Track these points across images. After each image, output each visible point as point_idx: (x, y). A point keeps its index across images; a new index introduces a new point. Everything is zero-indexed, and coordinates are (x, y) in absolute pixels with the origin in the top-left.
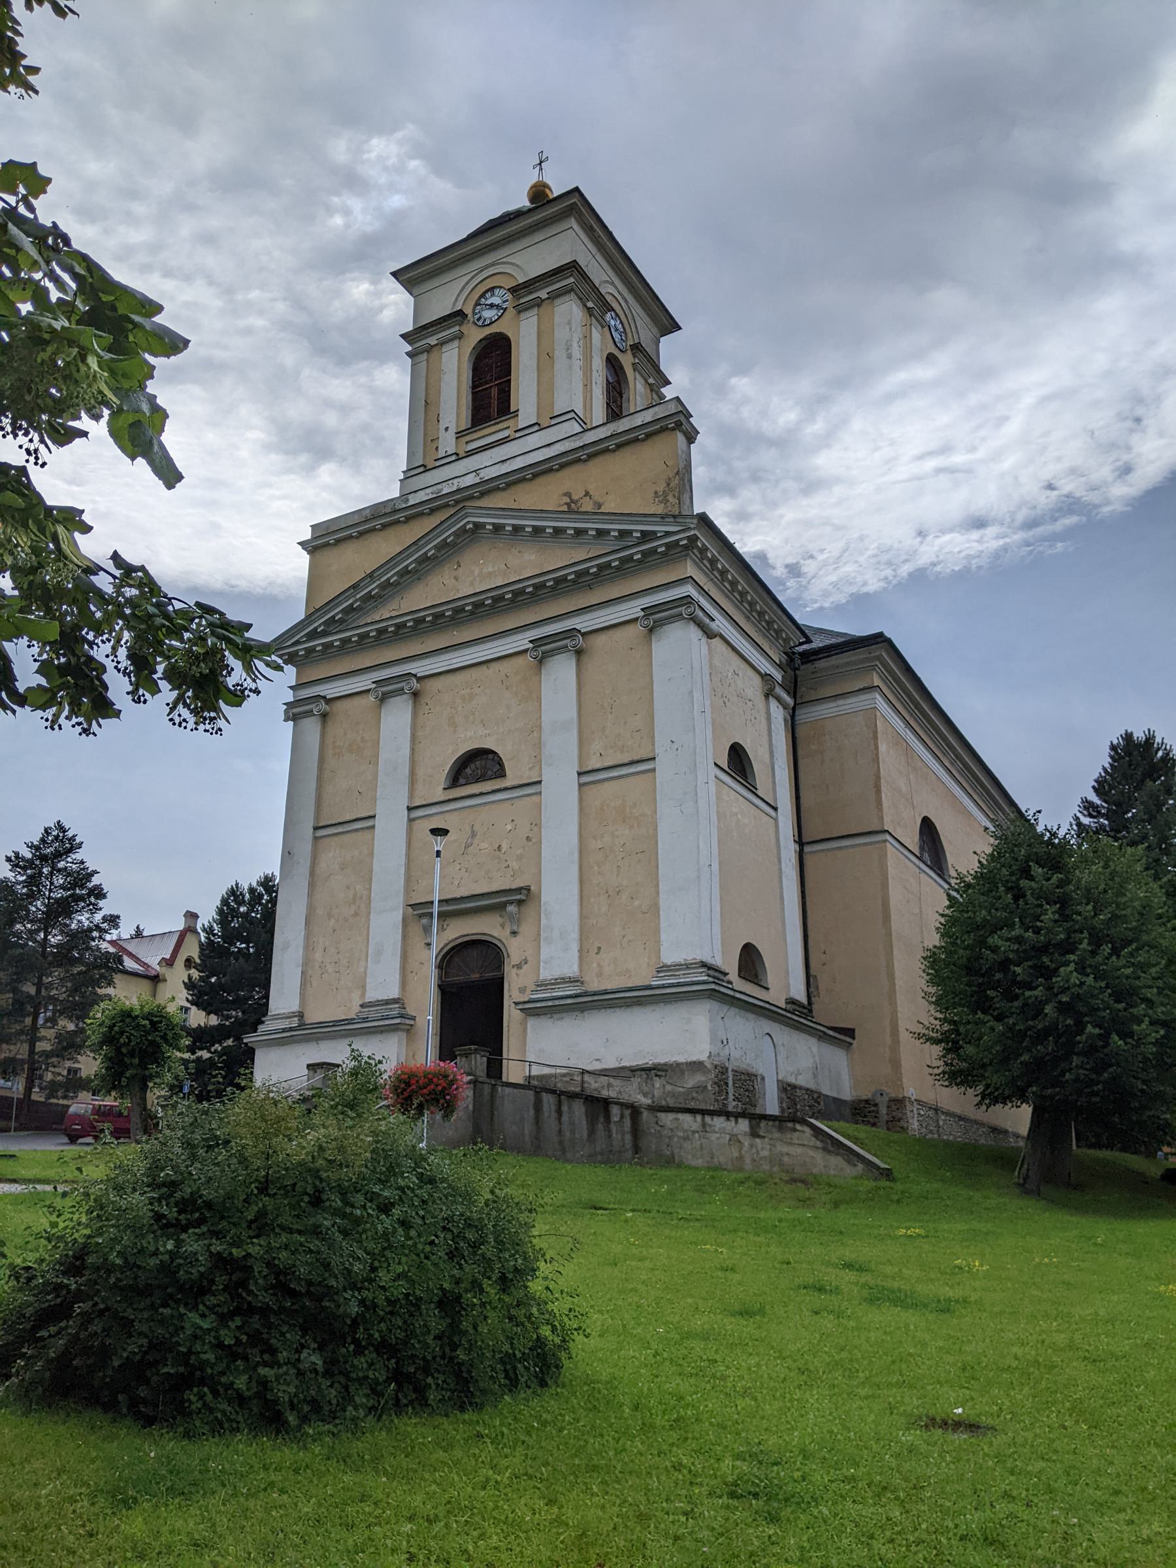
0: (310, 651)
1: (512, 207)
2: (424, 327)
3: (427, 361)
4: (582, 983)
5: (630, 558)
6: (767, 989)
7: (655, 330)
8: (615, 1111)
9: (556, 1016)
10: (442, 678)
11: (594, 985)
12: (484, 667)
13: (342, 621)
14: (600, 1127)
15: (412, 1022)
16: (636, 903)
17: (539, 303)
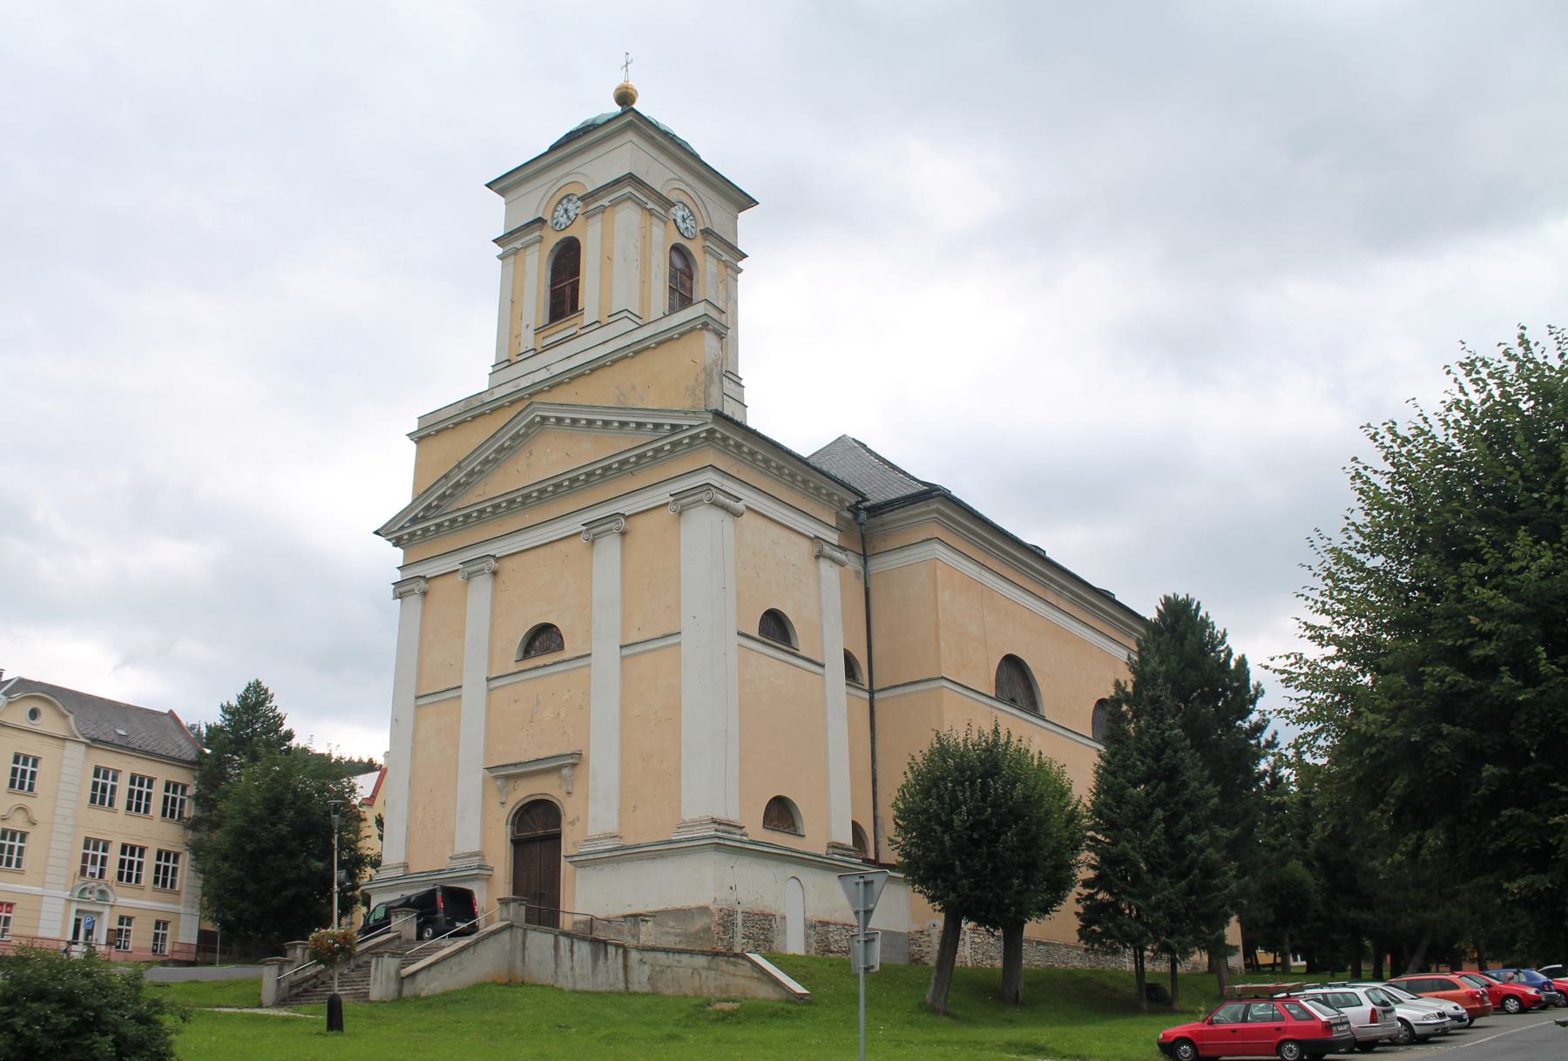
0: (413, 534)
2: (511, 233)
8: (611, 950)
11: (630, 840)
13: (437, 507)
14: (601, 963)
17: (603, 209)
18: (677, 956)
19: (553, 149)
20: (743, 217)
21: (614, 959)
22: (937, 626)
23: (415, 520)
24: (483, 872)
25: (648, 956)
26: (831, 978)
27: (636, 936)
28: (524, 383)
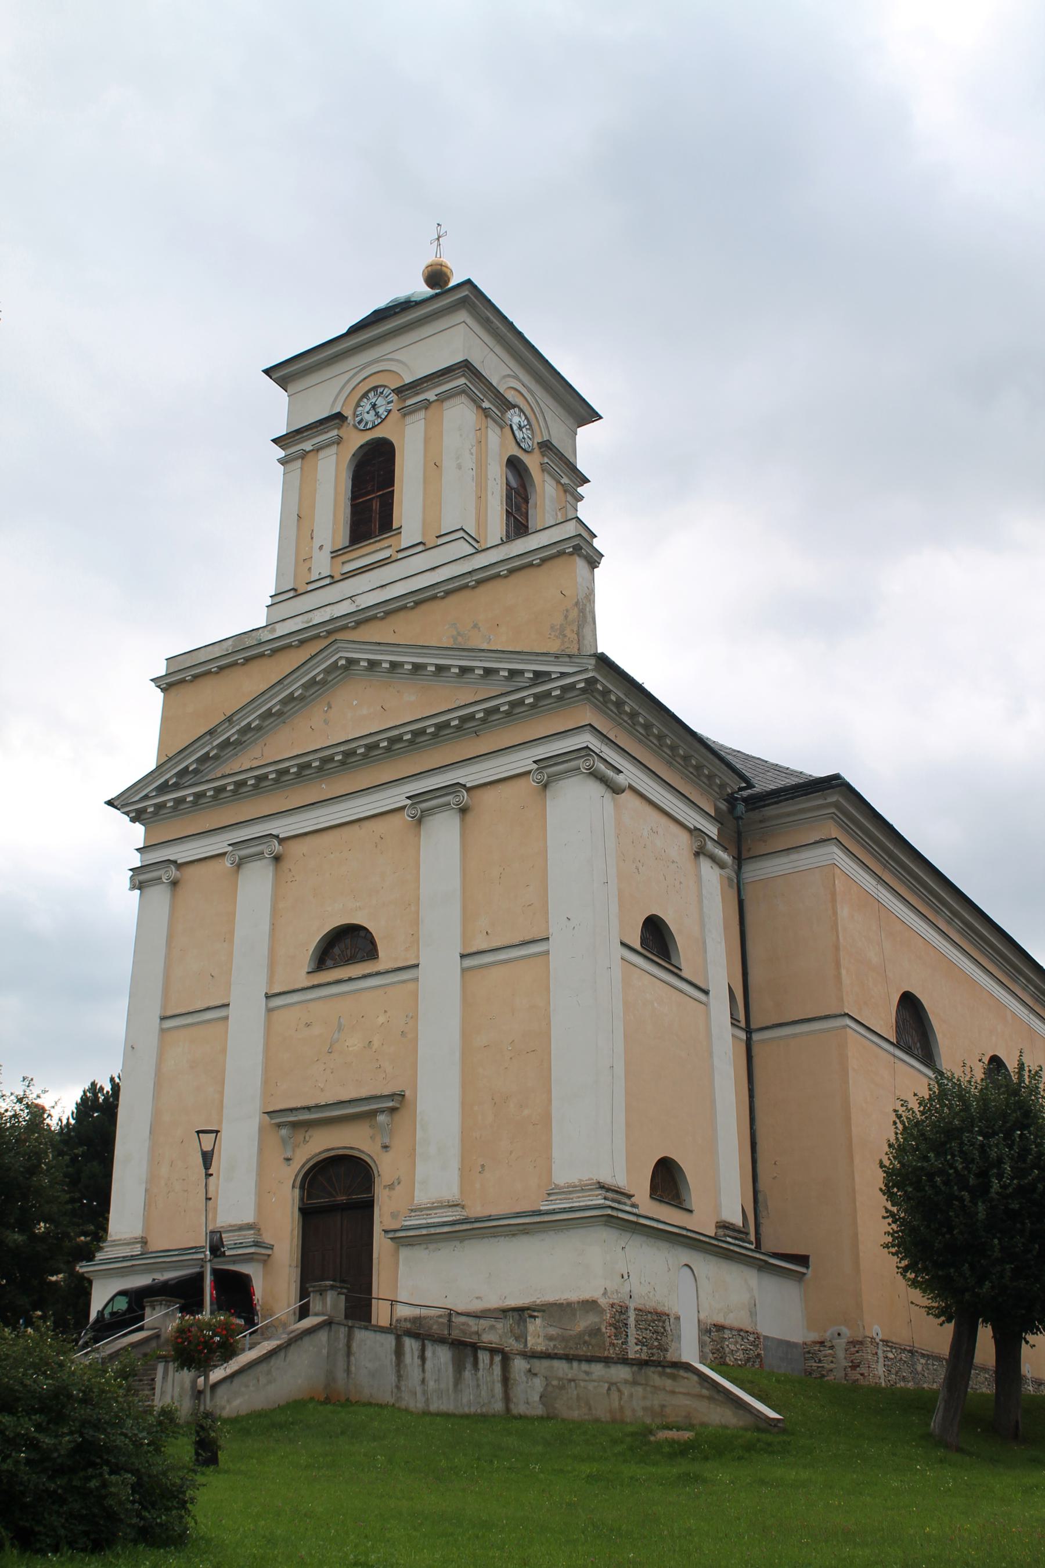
0: (160, 807)
1: (401, 292)
2: (298, 431)
3: (301, 468)
4: (463, 1207)
5: (521, 702)
6: (691, 1211)
7: (570, 421)
8: (484, 1357)
9: (432, 1247)
10: (308, 839)
11: (476, 1210)
12: (356, 826)
13: (196, 772)
14: (467, 1374)
15: (269, 1252)
16: (526, 1112)
17: (427, 405)
18: (585, 1366)
19: (354, 330)
20: (584, 433)
21: (489, 1370)
22: (837, 948)
23: (163, 788)
24: (261, 1252)
25: (541, 1366)
26: (820, 1403)
27: (521, 1337)
28: (318, 618)
